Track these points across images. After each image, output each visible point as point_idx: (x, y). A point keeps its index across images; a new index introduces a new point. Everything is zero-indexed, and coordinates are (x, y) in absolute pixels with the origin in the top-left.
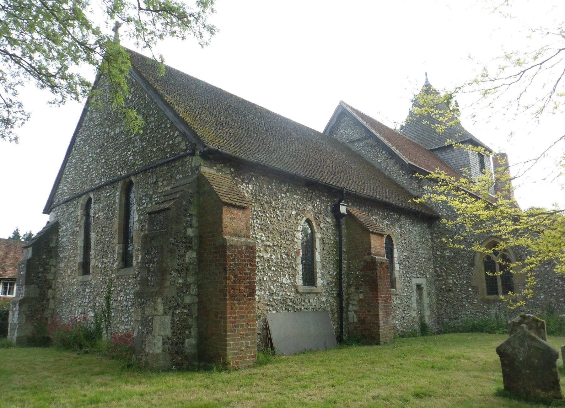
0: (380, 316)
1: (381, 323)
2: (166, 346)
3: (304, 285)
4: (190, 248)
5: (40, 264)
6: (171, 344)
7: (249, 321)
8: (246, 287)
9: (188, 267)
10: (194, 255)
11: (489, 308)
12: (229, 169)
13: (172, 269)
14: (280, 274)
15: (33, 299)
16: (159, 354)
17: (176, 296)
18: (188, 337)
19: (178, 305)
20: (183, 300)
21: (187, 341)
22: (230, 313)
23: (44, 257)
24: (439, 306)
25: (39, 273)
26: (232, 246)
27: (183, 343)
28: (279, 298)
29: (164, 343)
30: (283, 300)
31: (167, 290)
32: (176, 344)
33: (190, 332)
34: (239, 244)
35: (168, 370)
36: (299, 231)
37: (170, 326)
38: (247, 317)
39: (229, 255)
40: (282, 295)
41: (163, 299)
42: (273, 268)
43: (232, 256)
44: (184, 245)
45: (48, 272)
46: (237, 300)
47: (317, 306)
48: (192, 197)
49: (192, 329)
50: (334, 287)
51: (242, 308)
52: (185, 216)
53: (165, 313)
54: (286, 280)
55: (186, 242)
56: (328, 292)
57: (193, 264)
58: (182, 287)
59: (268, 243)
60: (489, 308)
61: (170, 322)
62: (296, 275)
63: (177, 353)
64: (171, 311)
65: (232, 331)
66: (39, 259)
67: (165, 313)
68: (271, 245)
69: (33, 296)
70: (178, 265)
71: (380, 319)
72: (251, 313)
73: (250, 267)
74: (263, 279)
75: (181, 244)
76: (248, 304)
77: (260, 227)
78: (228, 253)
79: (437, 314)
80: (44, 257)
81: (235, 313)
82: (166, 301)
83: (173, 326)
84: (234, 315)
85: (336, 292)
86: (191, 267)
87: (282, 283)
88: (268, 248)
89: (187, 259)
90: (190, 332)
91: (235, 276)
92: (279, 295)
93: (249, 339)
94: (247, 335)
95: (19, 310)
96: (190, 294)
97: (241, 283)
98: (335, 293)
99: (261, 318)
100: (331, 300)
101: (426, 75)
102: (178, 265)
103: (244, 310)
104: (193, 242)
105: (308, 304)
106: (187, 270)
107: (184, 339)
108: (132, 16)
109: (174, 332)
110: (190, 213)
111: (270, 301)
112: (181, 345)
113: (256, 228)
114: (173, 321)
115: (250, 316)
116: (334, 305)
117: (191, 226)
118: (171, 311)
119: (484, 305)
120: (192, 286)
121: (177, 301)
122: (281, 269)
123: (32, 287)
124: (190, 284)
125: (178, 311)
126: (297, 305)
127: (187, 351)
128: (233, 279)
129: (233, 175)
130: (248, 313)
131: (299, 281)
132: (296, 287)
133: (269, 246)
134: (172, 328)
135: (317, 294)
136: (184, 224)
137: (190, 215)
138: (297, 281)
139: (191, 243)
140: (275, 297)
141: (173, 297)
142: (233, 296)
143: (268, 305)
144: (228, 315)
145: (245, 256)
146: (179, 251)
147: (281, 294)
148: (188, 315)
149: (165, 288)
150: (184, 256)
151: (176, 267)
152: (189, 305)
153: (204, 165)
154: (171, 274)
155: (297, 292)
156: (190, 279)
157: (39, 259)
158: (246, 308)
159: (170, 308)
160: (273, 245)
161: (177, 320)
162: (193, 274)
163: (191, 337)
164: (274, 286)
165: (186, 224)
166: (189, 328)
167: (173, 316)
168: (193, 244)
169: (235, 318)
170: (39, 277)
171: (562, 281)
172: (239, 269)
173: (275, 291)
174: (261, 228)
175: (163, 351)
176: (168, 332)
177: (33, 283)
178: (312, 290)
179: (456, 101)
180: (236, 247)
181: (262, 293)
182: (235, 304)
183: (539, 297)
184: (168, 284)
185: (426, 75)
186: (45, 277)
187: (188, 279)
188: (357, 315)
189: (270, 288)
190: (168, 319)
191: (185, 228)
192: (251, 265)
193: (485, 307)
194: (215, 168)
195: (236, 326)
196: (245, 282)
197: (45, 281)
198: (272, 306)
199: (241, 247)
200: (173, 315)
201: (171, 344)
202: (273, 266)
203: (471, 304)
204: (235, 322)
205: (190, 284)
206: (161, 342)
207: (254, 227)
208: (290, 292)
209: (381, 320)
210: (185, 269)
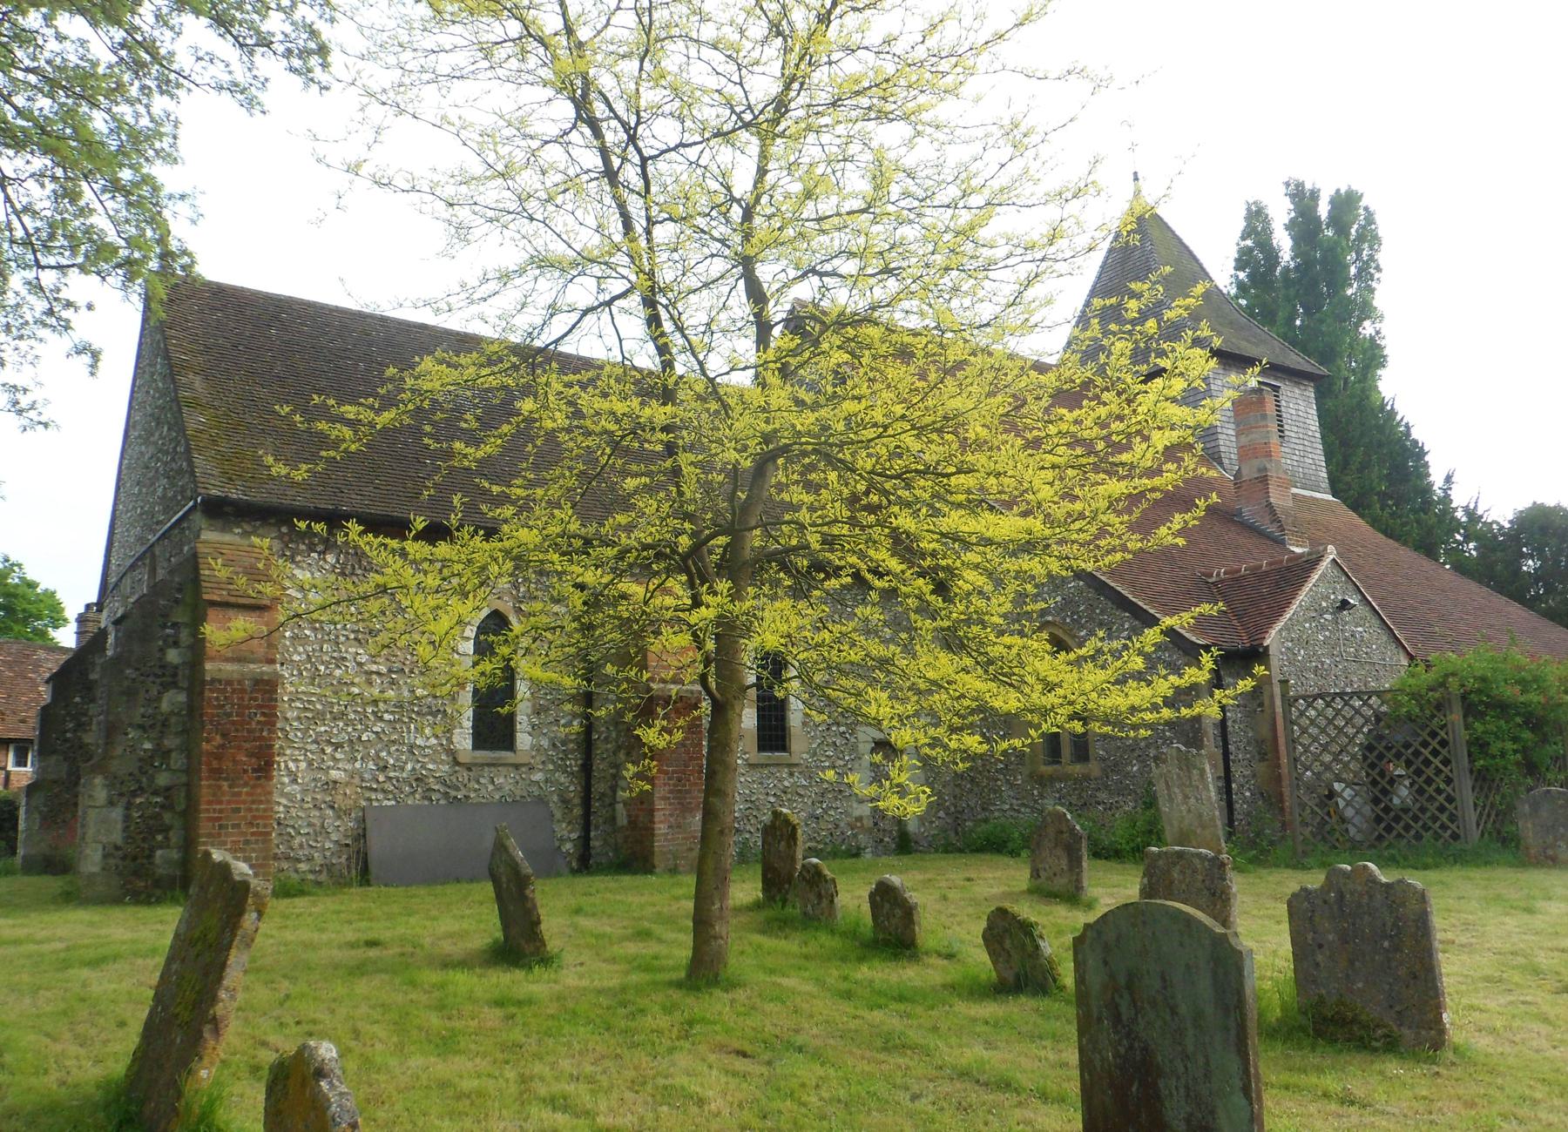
0: (658, 816)
1: (661, 828)
2: (112, 861)
3: (476, 747)
4: (174, 685)
5: (68, 714)
6: (124, 858)
7: (255, 817)
8: (251, 755)
9: (166, 720)
10: (182, 698)
11: (1041, 796)
12: (276, 529)
13: (130, 725)
14: (409, 728)
15: (55, 782)
16: (93, 875)
17: (136, 772)
18: (161, 848)
19: (141, 788)
20: (151, 779)
21: (159, 853)
22: (210, 803)
23: (77, 699)
24: (957, 791)
25: (66, 732)
26: (220, 681)
27: (150, 856)
28: (405, 775)
29: (105, 856)
30: (417, 780)
31: (115, 762)
32: (135, 859)
33: (166, 838)
34: (235, 676)
35: (117, 901)
36: (468, 639)
37: (120, 826)
38: (250, 810)
39: (210, 698)
40: (414, 769)
41: (106, 778)
42: (387, 717)
43: (217, 699)
44: (158, 681)
45: (86, 731)
46: (226, 779)
47: (518, 793)
48: (179, 590)
49: (171, 834)
50: (572, 752)
51: (239, 794)
52: (164, 626)
53: (111, 803)
54: (426, 738)
55: (164, 675)
56: (553, 763)
57: (178, 714)
58: (151, 757)
59: (374, 668)
60: (1041, 796)
61: (120, 818)
62: (455, 728)
63: (136, 873)
64: (124, 800)
65: (210, 835)
66: (67, 706)
67: (111, 803)
68: (384, 669)
69: (53, 777)
70: (143, 716)
71: (656, 820)
72: (261, 802)
73: (262, 719)
74: (360, 737)
75: (151, 679)
76: (254, 787)
77: (352, 636)
78: (207, 694)
79: (952, 809)
80: (77, 699)
81: (220, 802)
82: (113, 781)
83: (127, 827)
84: (218, 807)
85: (579, 762)
86: (173, 720)
87: (412, 747)
88: (374, 676)
89: (165, 706)
90: (166, 838)
91: (224, 735)
92: (403, 769)
93: (254, 850)
94: (247, 842)
95: (27, 804)
96: (168, 769)
97: (239, 748)
98: (574, 764)
99: (353, 815)
100: (562, 780)
101: (1136, 179)
102: (143, 716)
103: (244, 797)
104: (180, 673)
105: (491, 787)
106: (164, 725)
107: (152, 850)
108: (180, 203)
109: (128, 837)
110: (174, 620)
111: (378, 781)
112: (145, 861)
113: (342, 639)
114: (127, 818)
115: (257, 810)
116: (572, 788)
117: (176, 644)
118: (124, 800)
119: (1033, 788)
120: (174, 755)
121: (139, 781)
122: (411, 718)
123: (53, 759)
124: (170, 751)
125: (138, 801)
126: (458, 789)
127: (160, 871)
128: (218, 740)
129: (286, 539)
130: (253, 802)
131: (463, 740)
132: (452, 753)
133: (378, 673)
134: (126, 829)
135: (517, 767)
136: (160, 643)
137: (175, 625)
138: (454, 740)
139: (175, 675)
140: (392, 774)
141: (131, 774)
142: (216, 773)
143: (371, 789)
144: (203, 807)
145: (251, 699)
146: (147, 691)
147: (409, 767)
148: (163, 807)
149: (112, 758)
150: (159, 699)
151: (138, 720)
152: (168, 789)
153: (208, 529)
154: (126, 734)
155: (456, 762)
156: (170, 742)
157: (67, 706)
158: (248, 794)
159: (121, 795)
160: (390, 671)
161: (136, 815)
162: (177, 734)
163: (168, 847)
164: (389, 753)
165: (165, 641)
166: (166, 830)
167: (127, 808)
168: (180, 677)
169: (221, 811)
170: (66, 740)
171: (1169, 731)
172: (234, 723)
173: (391, 761)
174: (355, 639)
175: (104, 869)
176: (117, 837)
177: (54, 752)
178: (499, 758)
179: (1366, 209)
180: (229, 682)
181: (358, 765)
182: (220, 787)
183: (1129, 768)
184: (119, 751)
185: (1136, 179)
186: (80, 739)
187: (166, 742)
188: (628, 811)
189: (379, 757)
190: (117, 814)
191: (162, 650)
192: (263, 714)
193: (1035, 792)
194: (237, 531)
195: (221, 827)
196: (247, 745)
197: (81, 747)
198: (384, 791)
199: (239, 682)
200: (128, 806)
201: (124, 858)
202: (387, 711)
203: (1012, 786)
204: (219, 819)
205: (170, 751)
206: (100, 853)
207: (337, 637)
208: (435, 762)
209: (661, 822)
210: (159, 724)
